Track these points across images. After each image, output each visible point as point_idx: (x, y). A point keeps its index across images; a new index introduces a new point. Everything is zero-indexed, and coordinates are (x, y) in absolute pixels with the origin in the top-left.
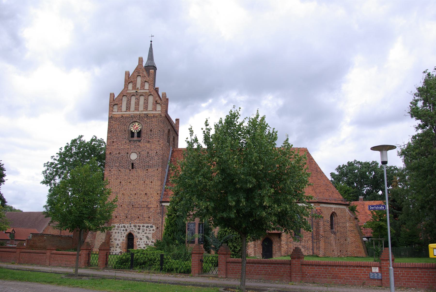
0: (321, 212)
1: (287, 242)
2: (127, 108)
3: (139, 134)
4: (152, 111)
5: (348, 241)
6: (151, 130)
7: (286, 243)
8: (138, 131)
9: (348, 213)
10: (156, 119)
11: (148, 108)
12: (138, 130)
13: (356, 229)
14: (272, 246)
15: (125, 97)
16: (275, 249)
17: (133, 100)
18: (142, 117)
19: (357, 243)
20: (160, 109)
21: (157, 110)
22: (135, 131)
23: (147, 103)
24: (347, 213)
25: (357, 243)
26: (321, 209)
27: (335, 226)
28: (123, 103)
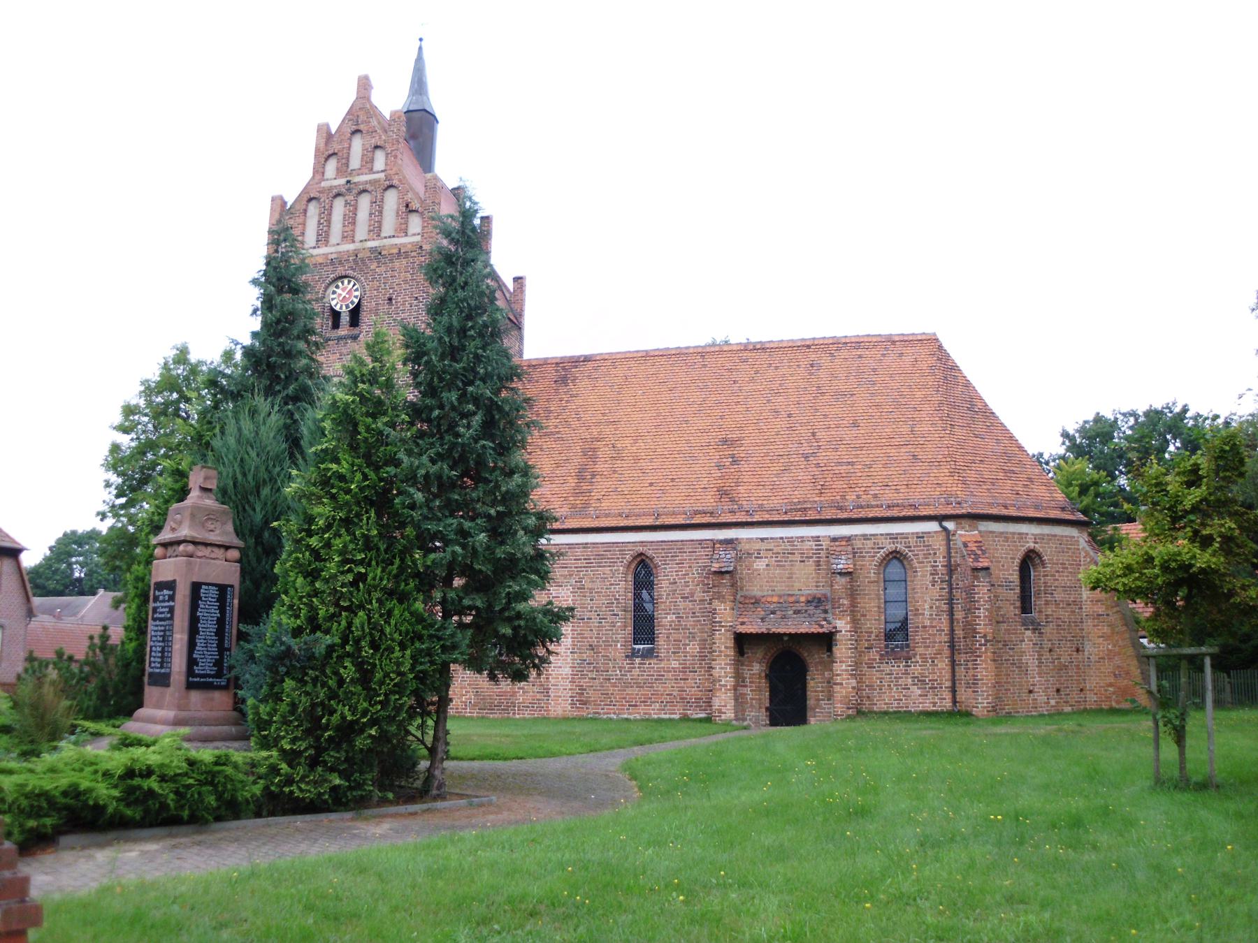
0: (979, 552)
1: (857, 664)
2: (319, 235)
3: (355, 313)
4: (394, 236)
5: (1086, 653)
6: (390, 299)
7: (852, 670)
8: (351, 307)
9: (1087, 554)
10: (404, 262)
11: (383, 230)
12: (352, 303)
13: (1115, 610)
14: (806, 679)
15: (313, 203)
16: (816, 691)
17: (339, 207)
18: (362, 260)
19: (1117, 661)
20: (419, 230)
21: (411, 231)
22: (341, 308)
23: (381, 212)
24: (1083, 554)
25: (1117, 661)
26: (980, 540)
27: (1037, 602)
28: (307, 224)
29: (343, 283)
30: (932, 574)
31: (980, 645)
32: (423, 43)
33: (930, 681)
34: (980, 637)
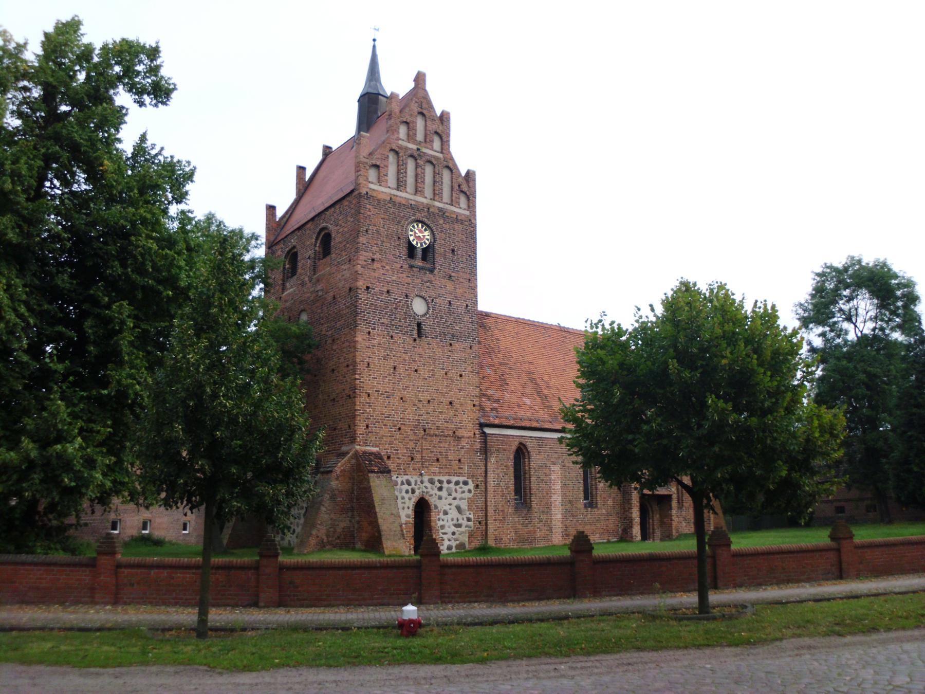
8: (424, 246)
29: (422, 227)
32: (376, 43)
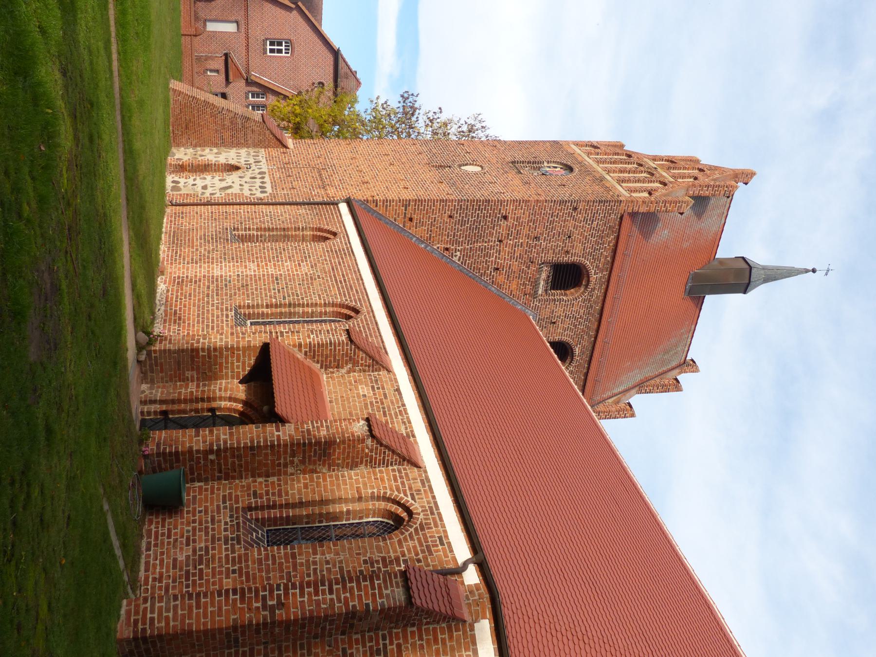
30: (384, 559)
31: (264, 597)
33: (201, 570)
34: (279, 596)
